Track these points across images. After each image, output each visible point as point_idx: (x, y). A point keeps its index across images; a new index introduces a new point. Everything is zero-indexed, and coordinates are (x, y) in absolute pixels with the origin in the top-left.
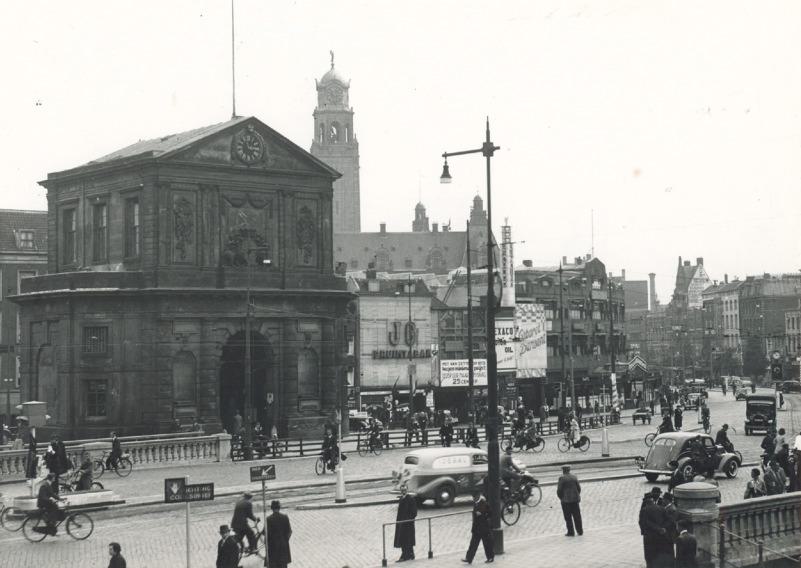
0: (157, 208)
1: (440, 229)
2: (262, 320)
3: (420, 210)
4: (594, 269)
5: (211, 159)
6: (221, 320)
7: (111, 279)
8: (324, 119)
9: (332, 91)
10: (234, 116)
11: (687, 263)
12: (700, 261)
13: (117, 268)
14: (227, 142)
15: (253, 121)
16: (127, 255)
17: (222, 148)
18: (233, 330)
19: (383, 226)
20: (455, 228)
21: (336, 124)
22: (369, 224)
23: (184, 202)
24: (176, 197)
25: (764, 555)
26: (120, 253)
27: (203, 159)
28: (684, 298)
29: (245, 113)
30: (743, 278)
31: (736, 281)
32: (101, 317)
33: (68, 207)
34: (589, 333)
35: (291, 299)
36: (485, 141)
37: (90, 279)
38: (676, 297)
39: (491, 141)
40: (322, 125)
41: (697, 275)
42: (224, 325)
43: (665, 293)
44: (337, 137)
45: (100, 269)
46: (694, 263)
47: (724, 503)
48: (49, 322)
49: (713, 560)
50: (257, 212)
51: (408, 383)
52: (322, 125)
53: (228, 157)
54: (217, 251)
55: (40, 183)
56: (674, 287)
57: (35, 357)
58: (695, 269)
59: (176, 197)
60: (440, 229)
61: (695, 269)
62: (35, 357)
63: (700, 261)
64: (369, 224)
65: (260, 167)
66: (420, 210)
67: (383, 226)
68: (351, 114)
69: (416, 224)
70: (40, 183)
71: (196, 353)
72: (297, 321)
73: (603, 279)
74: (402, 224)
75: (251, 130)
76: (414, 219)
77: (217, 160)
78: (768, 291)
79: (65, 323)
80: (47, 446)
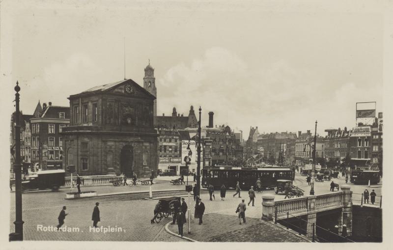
0: (102, 107)
1: (180, 116)
2: (132, 142)
3: (174, 109)
4: (227, 129)
5: (118, 92)
6: (121, 141)
7: (88, 128)
8: (146, 80)
9: (149, 71)
10: (125, 79)
11: (253, 128)
12: (257, 127)
13: (91, 124)
14: (123, 87)
15: (130, 80)
16: (93, 121)
17: (121, 89)
18: (124, 144)
19: (164, 114)
20: (184, 116)
21: (150, 82)
22: (159, 113)
23: (110, 105)
24: (108, 104)
25: (289, 216)
26: (91, 120)
27: (116, 92)
28: (252, 138)
29: (128, 78)
30: (269, 133)
31: (267, 134)
32: (86, 140)
33: (76, 106)
34: (225, 149)
35: (141, 136)
36: (14, 110)
37: (82, 128)
38: (249, 138)
39: (20, 109)
40: (146, 82)
41: (256, 132)
42: (121, 143)
43: (245, 137)
44: (150, 86)
45: (85, 125)
46: (255, 128)
47: (275, 200)
48: (71, 141)
49: (273, 217)
50: (132, 109)
51: (24, 197)
52: (146, 82)
53: (123, 92)
54: (120, 121)
55: (68, 98)
56: (249, 135)
57: (67, 150)
58: (255, 130)
59: (108, 104)
60: (180, 116)
61: (255, 130)
62: (67, 150)
63: (257, 127)
64: (159, 113)
65: (132, 95)
66: (174, 109)
67: (164, 114)
68: (155, 79)
69: (173, 114)
70: (68, 98)
71: (114, 151)
72: (142, 142)
73: (230, 132)
74: (169, 113)
75: (130, 83)
76: (190, 109)
77: (120, 92)
78: (277, 137)
79: (75, 141)
80: (210, 145)
